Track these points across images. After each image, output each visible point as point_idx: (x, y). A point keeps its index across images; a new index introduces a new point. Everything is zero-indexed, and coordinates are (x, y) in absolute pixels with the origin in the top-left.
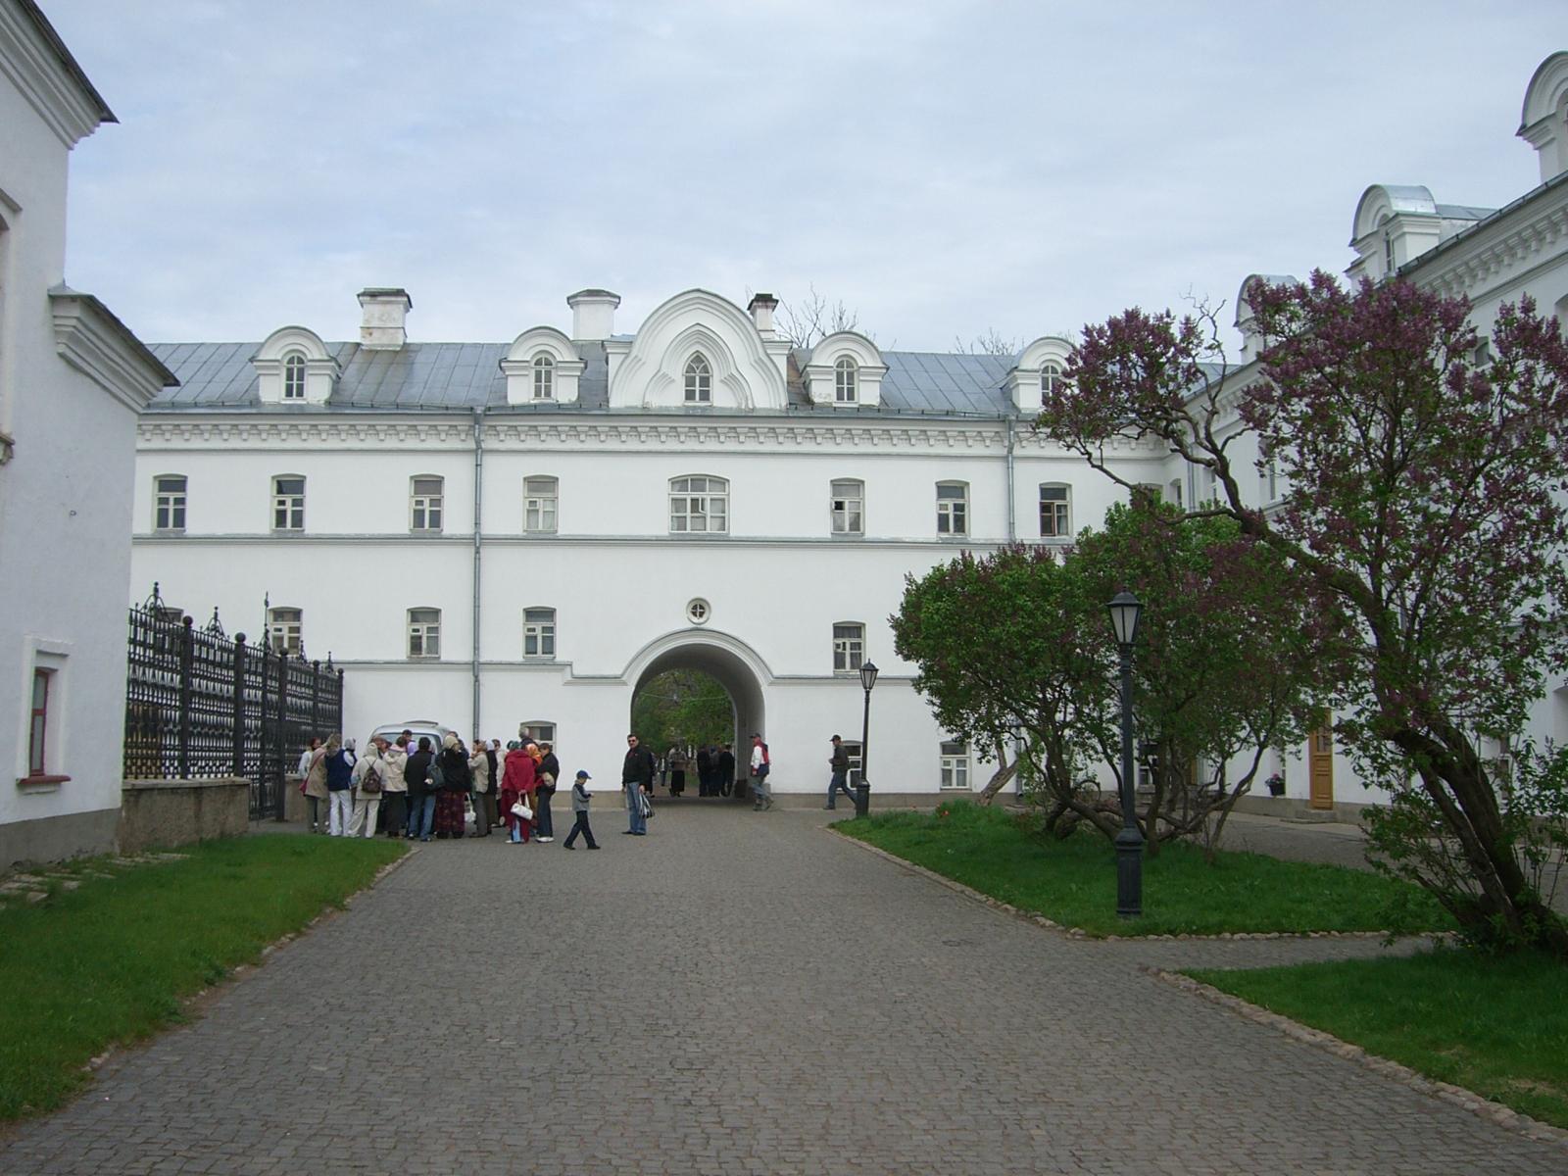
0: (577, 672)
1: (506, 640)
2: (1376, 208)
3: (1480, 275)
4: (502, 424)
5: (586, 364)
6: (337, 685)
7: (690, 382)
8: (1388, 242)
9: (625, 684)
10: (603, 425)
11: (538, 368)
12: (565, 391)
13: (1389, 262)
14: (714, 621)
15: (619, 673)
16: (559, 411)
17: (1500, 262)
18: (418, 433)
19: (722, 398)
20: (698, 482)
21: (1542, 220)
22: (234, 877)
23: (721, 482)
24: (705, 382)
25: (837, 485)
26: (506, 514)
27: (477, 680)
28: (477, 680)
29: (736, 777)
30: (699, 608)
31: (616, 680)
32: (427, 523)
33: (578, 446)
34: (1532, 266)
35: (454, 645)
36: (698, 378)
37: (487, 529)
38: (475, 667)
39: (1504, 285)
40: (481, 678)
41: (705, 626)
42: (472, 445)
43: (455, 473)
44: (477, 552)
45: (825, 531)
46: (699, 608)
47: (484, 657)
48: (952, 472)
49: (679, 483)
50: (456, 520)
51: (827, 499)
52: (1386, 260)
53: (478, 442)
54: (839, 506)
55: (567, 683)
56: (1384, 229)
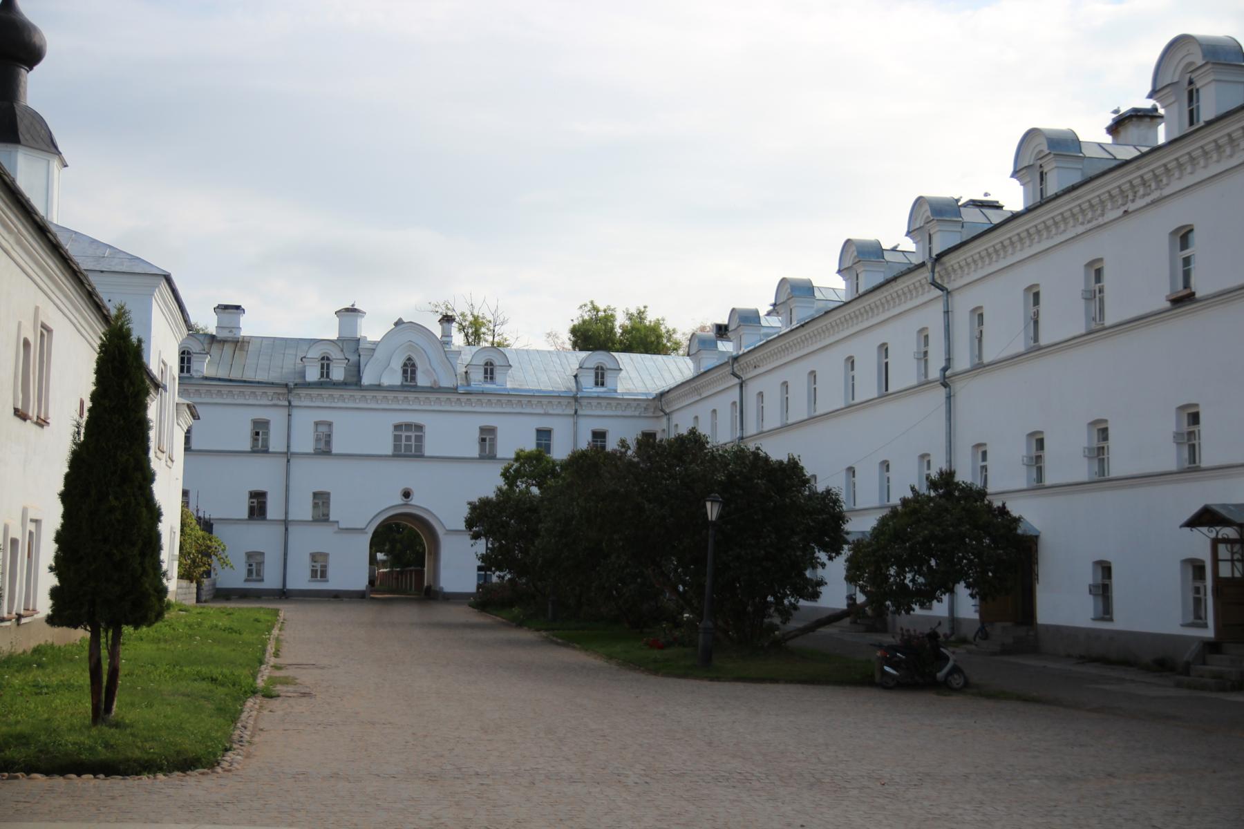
0: (342, 525)
1: (302, 509)
2: (921, 214)
3: (1165, 181)
4: (303, 392)
5: (349, 361)
6: (212, 525)
7: (405, 372)
8: (930, 235)
9: (367, 533)
10: (358, 394)
11: (323, 362)
12: (338, 374)
13: (1191, 112)
14: (415, 500)
15: (363, 527)
16: (336, 385)
17: (1032, 240)
18: (256, 396)
19: (422, 380)
20: (408, 426)
21: (1210, 143)
22: (508, 805)
23: (419, 428)
24: (413, 372)
25: (483, 430)
26: (304, 441)
27: (286, 529)
28: (286, 529)
29: (426, 584)
30: (407, 494)
31: (361, 531)
32: (324, 449)
33: (344, 405)
34: (837, 339)
35: (274, 510)
36: (409, 369)
37: (294, 449)
38: (286, 523)
39: (1004, 268)
40: (289, 529)
41: (410, 503)
42: (287, 403)
43: (276, 418)
44: (288, 461)
45: (476, 453)
46: (407, 494)
47: (291, 518)
48: (544, 423)
49: (397, 427)
50: (276, 442)
51: (476, 435)
52: (855, 282)
53: (290, 402)
54: (483, 440)
55: (335, 533)
56: (1039, 162)
